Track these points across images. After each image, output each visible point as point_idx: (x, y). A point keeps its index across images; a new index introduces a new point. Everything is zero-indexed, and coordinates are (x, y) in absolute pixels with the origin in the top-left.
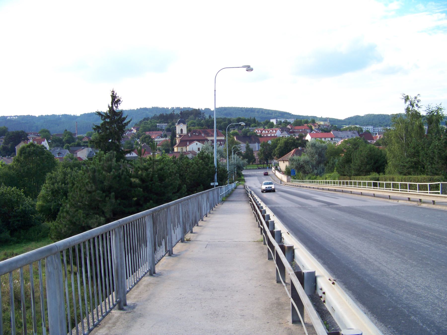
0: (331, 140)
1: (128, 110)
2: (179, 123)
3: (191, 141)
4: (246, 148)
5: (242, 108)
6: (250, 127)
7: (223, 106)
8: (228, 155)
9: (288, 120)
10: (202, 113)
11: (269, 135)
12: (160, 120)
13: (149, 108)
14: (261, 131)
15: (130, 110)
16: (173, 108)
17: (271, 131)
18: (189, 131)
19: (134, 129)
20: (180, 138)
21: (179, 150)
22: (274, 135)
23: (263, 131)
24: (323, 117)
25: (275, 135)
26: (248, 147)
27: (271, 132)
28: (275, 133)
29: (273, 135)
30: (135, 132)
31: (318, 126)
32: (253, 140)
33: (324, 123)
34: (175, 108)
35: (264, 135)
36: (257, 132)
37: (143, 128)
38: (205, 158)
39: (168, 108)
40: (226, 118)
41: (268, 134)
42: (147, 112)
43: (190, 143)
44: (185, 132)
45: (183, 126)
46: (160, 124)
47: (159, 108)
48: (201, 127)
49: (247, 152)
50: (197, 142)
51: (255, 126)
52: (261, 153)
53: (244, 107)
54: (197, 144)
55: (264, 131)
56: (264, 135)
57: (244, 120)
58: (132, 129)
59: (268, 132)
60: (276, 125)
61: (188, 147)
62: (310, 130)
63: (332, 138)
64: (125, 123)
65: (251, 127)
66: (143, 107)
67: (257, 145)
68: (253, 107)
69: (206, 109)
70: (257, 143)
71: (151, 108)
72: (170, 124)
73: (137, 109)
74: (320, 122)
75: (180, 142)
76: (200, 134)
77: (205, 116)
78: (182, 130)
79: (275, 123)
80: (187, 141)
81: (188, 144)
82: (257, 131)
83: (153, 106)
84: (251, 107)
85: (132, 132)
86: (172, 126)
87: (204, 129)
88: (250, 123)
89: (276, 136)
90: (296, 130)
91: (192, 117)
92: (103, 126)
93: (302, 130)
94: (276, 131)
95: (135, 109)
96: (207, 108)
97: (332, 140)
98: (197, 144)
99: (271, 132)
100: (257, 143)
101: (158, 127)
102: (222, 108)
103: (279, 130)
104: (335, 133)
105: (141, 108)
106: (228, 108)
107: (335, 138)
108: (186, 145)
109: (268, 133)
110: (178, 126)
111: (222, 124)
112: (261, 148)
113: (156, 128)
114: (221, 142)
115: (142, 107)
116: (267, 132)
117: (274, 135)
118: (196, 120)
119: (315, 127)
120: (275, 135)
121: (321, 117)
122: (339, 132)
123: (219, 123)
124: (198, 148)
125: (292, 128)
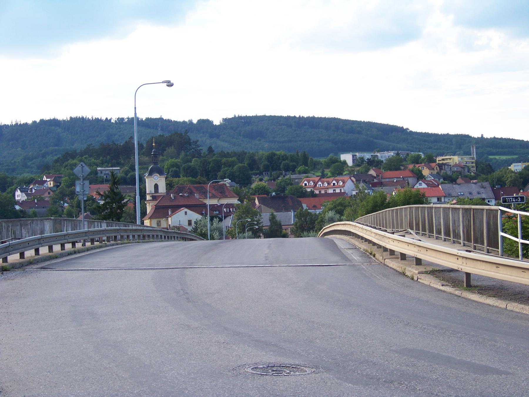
0: (438, 200)
1: (12, 126)
2: (151, 174)
3: (176, 208)
4: (270, 220)
5: (289, 117)
6: (295, 174)
7: (243, 114)
8: (449, 237)
9: (379, 155)
10: (193, 142)
11: (331, 191)
12: (101, 158)
13: (64, 121)
14: (314, 183)
15: (17, 124)
16: (123, 119)
17: (334, 182)
18: (169, 186)
19: (48, 180)
20: (155, 203)
21: (154, 225)
22: (341, 190)
23: (318, 182)
24: (485, 136)
25: (342, 191)
26: (273, 219)
27: (334, 184)
28: (343, 187)
29: (338, 191)
30: (52, 185)
31: (438, 168)
32: (291, 204)
33: (460, 159)
34: (126, 120)
35: (320, 192)
36: (306, 184)
37: (69, 178)
38: (203, 235)
39: (110, 120)
40: (245, 153)
41: (328, 188)
42: (60, 130)
43: (173, 212)
44: (162, 189)
45: (159, 179)
46: (103, 169)
47: (88, 119)
48: (194, 179)
49: (271, 226)
50: (186, 210)
51: (305, 172)
52: (297, 228)
53: (292, 115)
54: (186, 213)
55: (320, 183)
56: (320, 192)
57: (283, 157)
58: (45, 178)
59: (329, 184)
60: (351, 167)
61: (170, 219)
62: (416, 180)
63: (441, 198)
64: (124, 203)
65: (297, 172)
66: (47, 117)
67: (292, 214)
68: (316, 116)
69: (201, 122)
70: (292, 211)
71: (69, 119)
72: (126, 168)
73: (34, 122)
74: (452, 157)
75: (156, 209)
76: (191, 193)
77: (199, 149)
78: (156, 187)
79: (350, 163)
80: (168, 207)
81: (170, 213)
82: (306, 182)
83: (74, 116)
84: (311, 116)
85: (45, 185)
86: (130, 172)
87: (200, 183)
88: (294, 163)
89: (344, 193)
90: (387, 180)
91: (171, 150)
92: (104, 206)
93: (399, 179)
94: (344, 182)
95: (30, 122)
96: (205, 118)
97: (441, 201)
98: (186, 213)
99: (334, 184)
100: (292, 211)
101: (99, 175)
102: (240, 118)
103: (349, 181)
104: (446, 187)
105: (42, 121)
106: (256, 117)
107: (445, 197)
108: (166, 216)
109: (329, 186)
110: (150, 179)
111: (235, 167)
112: (297, 219)
113: (97, 177)
114: (231, 209)
115: (47, 117)
116: (326, 185)
117: (341, 190)
118: (181, 157)
119: (432, 171)
120: (342, 191)
121: (480, 136)
122: (454, 186)
123: (230, 166)
124: (189, 221)
125: (379, 176)
